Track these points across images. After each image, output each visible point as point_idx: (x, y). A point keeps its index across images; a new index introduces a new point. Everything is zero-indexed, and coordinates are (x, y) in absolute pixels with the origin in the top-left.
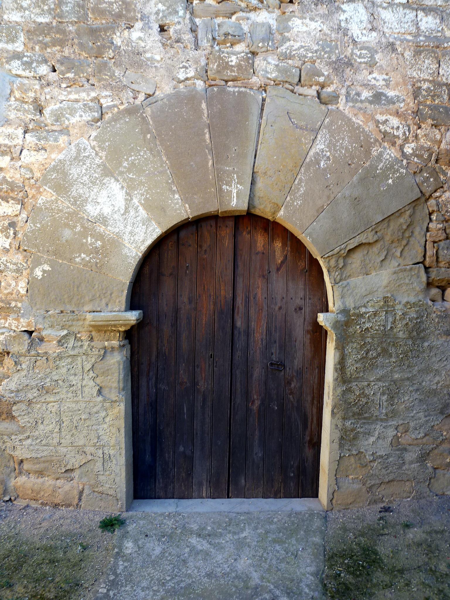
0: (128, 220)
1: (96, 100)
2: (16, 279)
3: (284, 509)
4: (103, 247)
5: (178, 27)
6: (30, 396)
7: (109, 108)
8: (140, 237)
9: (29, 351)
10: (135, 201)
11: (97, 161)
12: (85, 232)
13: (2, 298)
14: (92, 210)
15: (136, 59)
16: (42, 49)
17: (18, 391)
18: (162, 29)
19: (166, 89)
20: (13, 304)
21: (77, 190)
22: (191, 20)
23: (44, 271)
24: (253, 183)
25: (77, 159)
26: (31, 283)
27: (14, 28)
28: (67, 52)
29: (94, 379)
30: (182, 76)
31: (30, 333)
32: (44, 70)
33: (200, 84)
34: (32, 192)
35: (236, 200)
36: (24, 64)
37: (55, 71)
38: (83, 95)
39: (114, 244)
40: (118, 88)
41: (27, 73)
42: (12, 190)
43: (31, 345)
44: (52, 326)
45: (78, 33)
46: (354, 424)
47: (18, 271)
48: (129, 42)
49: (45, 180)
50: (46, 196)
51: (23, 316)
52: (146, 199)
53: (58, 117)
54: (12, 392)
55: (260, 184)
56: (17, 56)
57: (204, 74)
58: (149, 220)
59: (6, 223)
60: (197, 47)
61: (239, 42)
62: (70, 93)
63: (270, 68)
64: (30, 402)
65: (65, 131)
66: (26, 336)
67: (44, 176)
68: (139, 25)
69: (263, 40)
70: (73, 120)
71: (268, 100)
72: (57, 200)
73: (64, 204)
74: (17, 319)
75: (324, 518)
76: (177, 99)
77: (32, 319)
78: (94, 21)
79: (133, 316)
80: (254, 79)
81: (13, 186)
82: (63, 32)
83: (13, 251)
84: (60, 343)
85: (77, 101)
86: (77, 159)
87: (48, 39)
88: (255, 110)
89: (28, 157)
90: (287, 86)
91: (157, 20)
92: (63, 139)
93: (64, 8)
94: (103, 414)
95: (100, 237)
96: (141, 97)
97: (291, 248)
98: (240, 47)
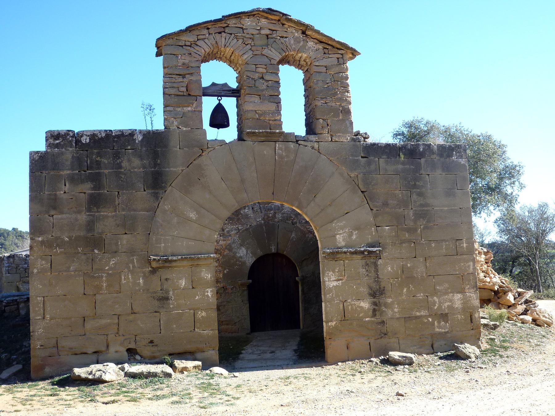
0: (246, 256)
14: (238, 255)
15: (247, 216)
19: (255, 224)
26: (224, 274)
35: (273, 249)
39: (244, 263)
40: (243, 225)
48: (245, 213)
49: (226, 248)
50: (227, 252)
53: (228, 232)
57: (263, 219)
60: (261, 212)
65: (230, 236)
73: (231, 254)
79: (250, 281)
86: (234, 243)
92: (230, 238)
95: (240, 261)
96: (249, 226)
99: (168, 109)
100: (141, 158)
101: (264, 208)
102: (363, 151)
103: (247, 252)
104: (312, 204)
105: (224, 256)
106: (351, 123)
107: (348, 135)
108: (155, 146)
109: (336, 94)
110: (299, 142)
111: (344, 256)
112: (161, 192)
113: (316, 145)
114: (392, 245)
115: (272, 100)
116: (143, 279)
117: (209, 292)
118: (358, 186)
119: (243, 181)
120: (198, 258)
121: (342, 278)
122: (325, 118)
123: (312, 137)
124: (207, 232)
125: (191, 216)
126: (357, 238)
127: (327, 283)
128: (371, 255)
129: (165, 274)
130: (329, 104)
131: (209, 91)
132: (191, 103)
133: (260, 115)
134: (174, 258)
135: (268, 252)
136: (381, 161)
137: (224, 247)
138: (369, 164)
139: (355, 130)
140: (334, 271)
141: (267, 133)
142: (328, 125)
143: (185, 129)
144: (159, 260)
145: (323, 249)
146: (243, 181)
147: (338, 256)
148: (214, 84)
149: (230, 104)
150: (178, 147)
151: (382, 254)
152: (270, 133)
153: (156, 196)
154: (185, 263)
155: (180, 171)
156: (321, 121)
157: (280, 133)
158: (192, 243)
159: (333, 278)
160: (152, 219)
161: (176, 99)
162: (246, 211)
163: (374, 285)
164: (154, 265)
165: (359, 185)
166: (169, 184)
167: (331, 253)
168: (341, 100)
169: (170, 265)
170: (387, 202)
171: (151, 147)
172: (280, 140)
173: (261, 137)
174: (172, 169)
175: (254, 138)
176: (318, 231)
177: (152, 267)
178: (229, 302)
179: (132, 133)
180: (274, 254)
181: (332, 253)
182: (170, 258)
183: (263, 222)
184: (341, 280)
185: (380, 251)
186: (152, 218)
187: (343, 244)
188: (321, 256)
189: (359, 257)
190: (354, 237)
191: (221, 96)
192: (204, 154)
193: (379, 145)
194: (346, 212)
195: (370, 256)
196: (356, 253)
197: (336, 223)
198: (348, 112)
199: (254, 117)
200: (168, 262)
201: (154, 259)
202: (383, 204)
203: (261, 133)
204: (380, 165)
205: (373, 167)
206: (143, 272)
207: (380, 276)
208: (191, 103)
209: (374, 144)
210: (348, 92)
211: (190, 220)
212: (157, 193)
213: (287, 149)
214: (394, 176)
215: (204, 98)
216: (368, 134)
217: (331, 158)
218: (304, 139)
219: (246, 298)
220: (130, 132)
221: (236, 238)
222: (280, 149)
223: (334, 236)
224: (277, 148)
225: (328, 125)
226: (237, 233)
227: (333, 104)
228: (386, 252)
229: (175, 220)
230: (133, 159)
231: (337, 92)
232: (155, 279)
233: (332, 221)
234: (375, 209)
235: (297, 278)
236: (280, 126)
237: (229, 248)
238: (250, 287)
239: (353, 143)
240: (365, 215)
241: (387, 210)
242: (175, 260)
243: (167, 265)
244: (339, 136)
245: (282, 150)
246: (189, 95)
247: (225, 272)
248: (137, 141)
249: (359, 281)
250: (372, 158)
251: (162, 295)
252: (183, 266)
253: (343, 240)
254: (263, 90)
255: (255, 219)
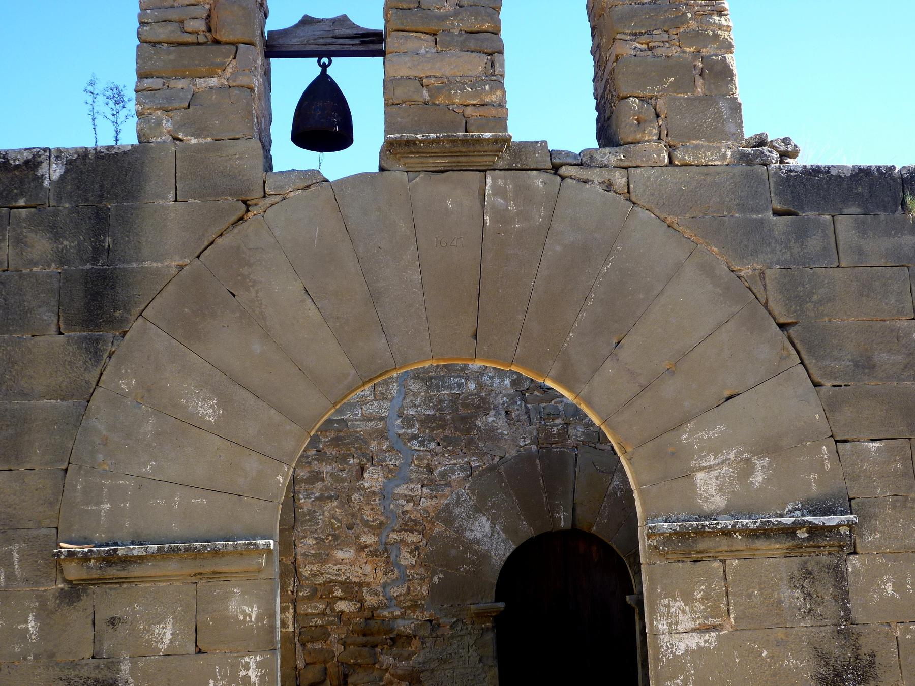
0: (491, 538)
1: (468, 463)
2: (420, 585)
3: (470, 73)
4: (478, 559)
5: (517, 412)
6: (432, 666)
7: (477, 467)
8: (501, 552)
9: (431, 634)
10: (497, 527)
12: (465, 550)
14: (469, 536)
15: (492, 434)
16: (430, 432)
17: (424, 663)
18: (507, 412)
19: (514, 453)
20: (419, 602)
21: (459, 523)
22: (526, 406)
23: (439, 579)
24: (574, 510)
26: (432, 587)
27: (411, 419)
28: (446, 433)
29: (476, 651)
30: (522, 444)
31: (430, 621)
32: (432, 445)
33: (534, 447)
34: (428, 526)
35: (563, 520)
36: (419, 442)
37: (439, 445)
38: (460, 460)
39: (484, 557)
40: (482, 455)
41: (422, 448)
42: (416, 525)
43: (432, 630)
44: (446, 616)
45: (453, 419)
46: (382, 435)
47: (421, 579)
48: (486, 424)
49: (438, 517)
50: (439, 527)
51: (426, 610)
52: (504, 526)
53: (443, 475)
54: (420, 663)
55: (578, 511)
56: (414, 437)
57: (536, 441)
58: (507, 539)
59: (413, 548)
60: (530, 423)
61: (557, 418)
62: (450, 460)
63: (579, 434)
64: (433, 671)
65: (448, 484)
66: (429, 624)
67: (437, 515)
68: (492, 412)
69: (573, 416)
70: (454, 477)
71: (579, 456)
72: (446, 530)
73: (451, 533)
74: (422, 613)
76: (519, 458)
77: (432, 612)
78: (462, 411)
79: (501, 605)
80: (569, 442)
81: (416, 522)
82: (444, 420)
83: (417, 566)
84: (452, 626)
85: (455, 465)
86: (458, 502)
87: (434, 425)
88: (572, 462)
90: (591, 445)
91: (504, 408)
92: (447, 490)
93: (444, 405)
94: (483, 676)
95: (475, 553)
96: (497, 459)
97: (721, 139)
98: (558, 421)
99: (147, 83)
100: (55, 231)
101: (538, 411)
102: (779, 194)
103: (493, 528)
104: (609, 369)
105: (432, 539)
106: (736, 107)
107: (724, 143)
108: (101, 196)
109: (681, 19)
110: (563, 170)
111: (724, 544)
112: (109, 335)
113: (619, 180)
114: (894, 507)
115: (472, 45)
116: (36, 619)
117: (253, 665)
118: (766, 306)
119: (374, 297)
120: (216, 552)
121: (717, 621)
122: (647, 93)
123: (611, 156)
124: (252, 464)
125: (202, 411)
126: (767, 481)
127: (665, 640)
128: (820, 541)
129: (106, 602)
130: (658, 52)
131: (294, 42)
132: (218, 66)
133: (434, 92)
134: (137, 551)
135: (548, 529)
136: (843, 222)
137: (432, 514)
138: (801, 233)
139: (749, 131)
140: (688, 598)
141: (454, 141)
142: (658, 116)
143: (194, 141)
144: (86, 558)
145: (652, 523)
146: (374, 297)
147: (703, 545)
148: (307, 21)
149: (361, 83)
150: (171, 195)
151: (861, 535)
152: (464, 142)
153: (94, 351)
154: (171, 567)
155: (174, 271)
156: (634, 102)
157: (495, 141)
158: (199, 501)
159: (686, 623)
160: (78, 423)
161: (173, 55)
162: (490, 419)
163: (835, 648)
164: (73, 571)
165: (771, 304)
166: (135, 312)
167: (676, 533)
168: (698, 37)
169: (122, 574)
170: (869, 358)
171: (87, 200)
172: (501, 164)
173: (435, 155)
174: (147, 264)
175: (413, 161)
176: (629, 460)
177: (65, 581)
178: (443, 661)
179: (33, 161)
180: (564, 532)
181: (682, 535)
182: (122, 551)
183: (534, 447)
184: (715, 628)
185: (850, 525)
186: (78, 419)
187: (719, 502)
188: (644, 543)
189: (778, 546)
190: (758, 478)
191: (331, 54)
192: (250, 215)
193: (834, 172)
194: (727, 393)
195: (819, 542)
196: (764, 532)
197: (692, 432)
198: (724, 74)
199: (416, 97)
200: (111, 566)
201: (71, 554)
202: (856, 366)
203: (432, 141)
204: (840, 237)
205: (814, 243)
206: (40, 597)
207: (858, 615)
208: (218, 66)
209: (816, 171)
210: (721, 13)
211: (199, 425)
212: (97, 340)
213: (524, 194)
214: (890, 271)
215: (276, 64)
216: (794, 141)
217: (670, 219)
218: (583, 161)
219: (490, 650)
220: (27, 155)
221: (464, 491)
222: (497, 192)
223: (688, 476)
224: (488, 191)
225: (658, 116)
226: (465, 479)
227: (674, 51)
228: (874, 530)
229: (150, 425)
230: (33, 235)
231: (685, 14)
232: (76, 619)
233: (678, 426)
234: (828, 384)
235: (627, 597)
236: (501, 122)
237: (447, 516)
238: (501, 622)
239: (744, 168)
240: (791, 401)
241: (872, 384)
242: (141, 557)
243: (113, 572)
244: (697, 147)
245: (504, 197)
246: (217, 42)
247: (436, 580)
248: (46, 183)
249: (780, 634)
250: (810, 214)
251: (96, 674)
252: (169, 579)
253: (720, 489)
254: (444, 18)
255: (514, 440)
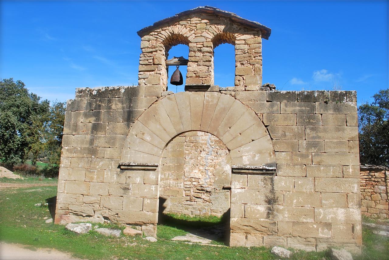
11: (226, 161)
13: (4, 135)
14: (225, 169)
25: (223, 161)
50: (218, 167)
73: (220, 168)
75: (308, 120)
84: (219, 190)
86: (223, 161)
89: (215, 161)
95: (226, 173)
